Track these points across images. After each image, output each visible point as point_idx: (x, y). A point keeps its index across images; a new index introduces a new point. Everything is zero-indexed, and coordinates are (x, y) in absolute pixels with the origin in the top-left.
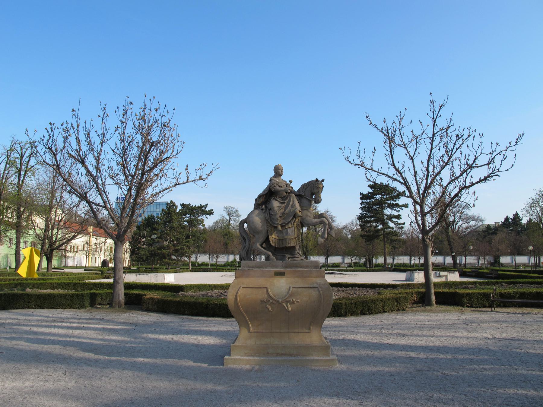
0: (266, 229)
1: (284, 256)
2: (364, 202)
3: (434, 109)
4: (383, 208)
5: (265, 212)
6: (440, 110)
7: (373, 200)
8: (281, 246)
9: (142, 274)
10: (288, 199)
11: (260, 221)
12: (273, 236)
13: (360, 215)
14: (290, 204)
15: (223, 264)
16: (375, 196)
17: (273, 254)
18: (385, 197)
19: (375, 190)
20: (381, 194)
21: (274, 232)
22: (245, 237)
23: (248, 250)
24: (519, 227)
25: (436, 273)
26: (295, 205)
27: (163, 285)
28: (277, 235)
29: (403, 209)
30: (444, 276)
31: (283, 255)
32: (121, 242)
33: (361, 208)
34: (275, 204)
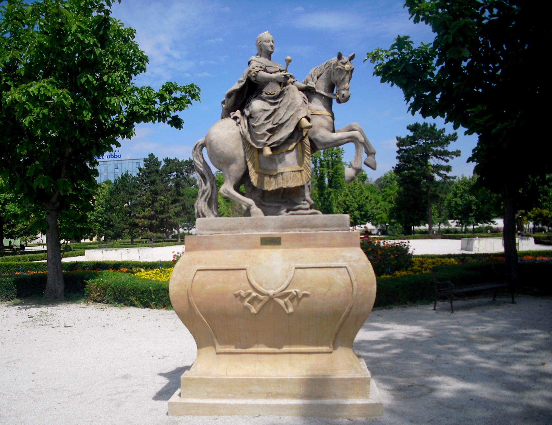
2: (402, 150)
16: (416, 141)
17: (259, 205)
22: (205, 174)
23: (210, 199)
33: (397, 157)
34: (257, 105)
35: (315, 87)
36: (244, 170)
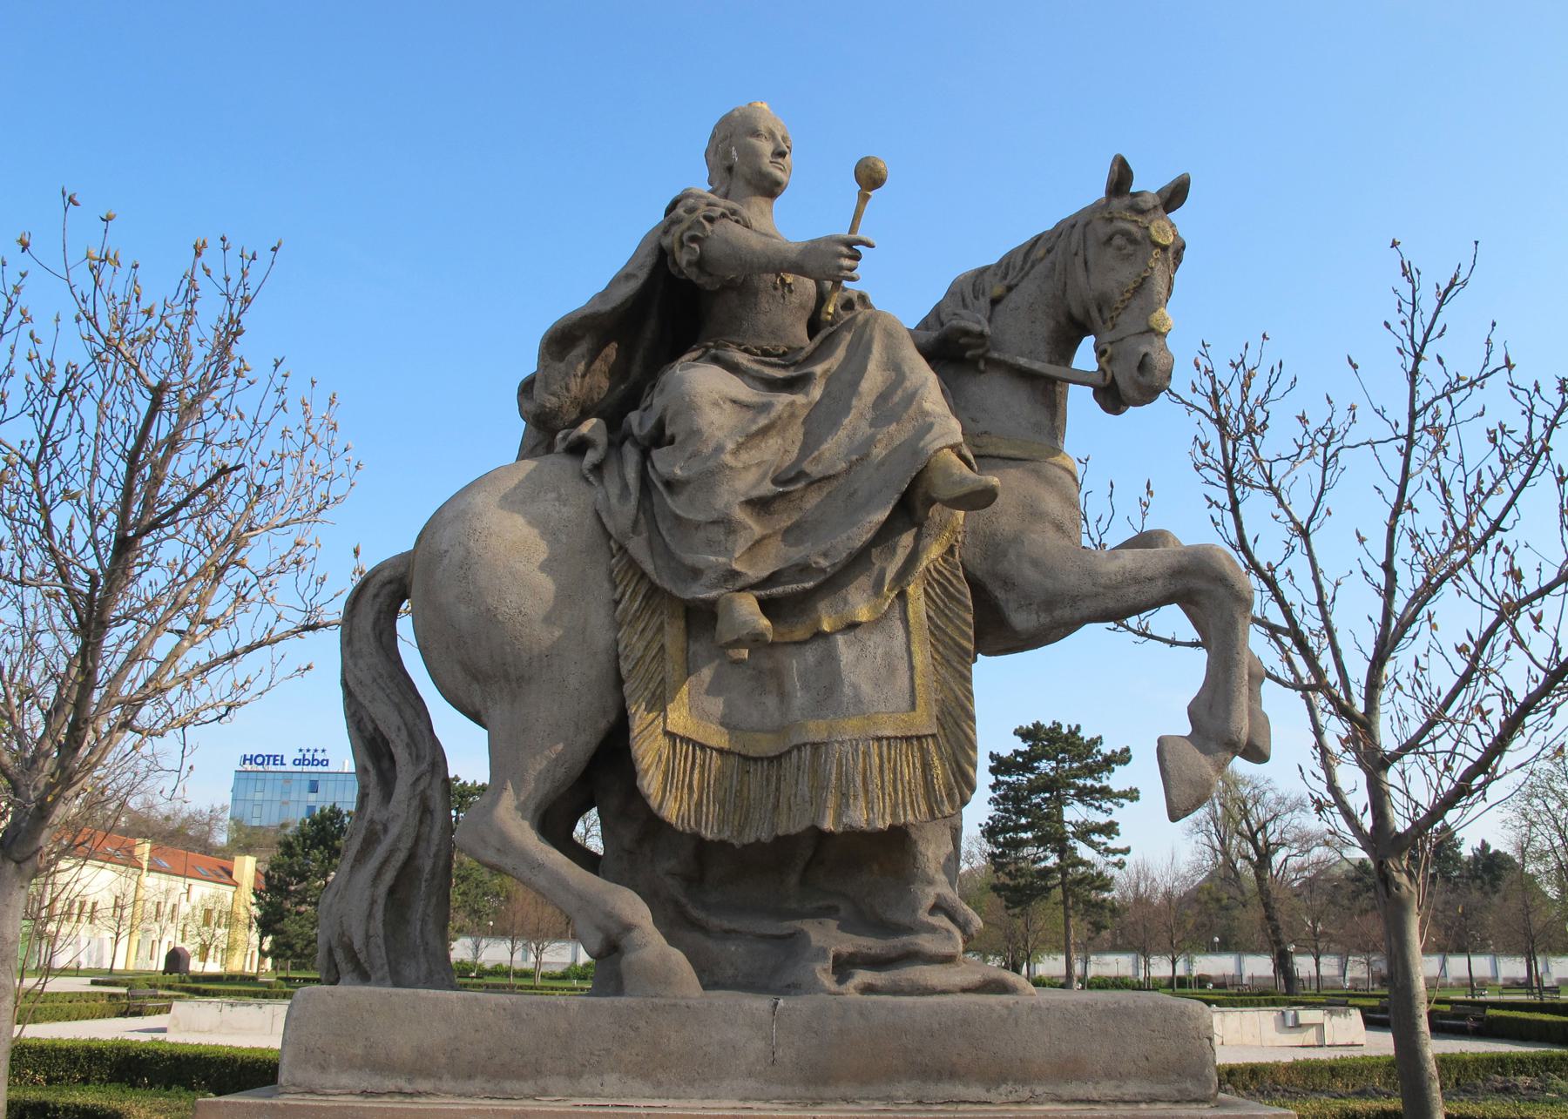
0: (601, 637)
1: (792, 944)
2: (1004, 783)
3: (1414, 304)
4: (1061, 802)
5: (598, 469)
6: (1441, 303)
7: (1032, 777)
8: (758, 832)
9: (243, 1005)
10: (840, 353)
11: (541, 551)
12: (679, 717)
13: (991, 823)
14: (865, 386)
15: (558, 970)
16: (1036, 764)
17: (674, 922)
18: (1067, 766)
19: (1037, 745)
20: (1055, 758)
21: (689, 670)
22: (391, 735)
23: (408, 870)
24: (1455, 867)
25: (1283, 1013)
26: (911, 397)
27: (257, 1060)
28: (716, 706)
29: (1122, 805)
30: (1312, 1025)
31: (787, 926)
32: (18, 862)
33: (992, 800)
35: (987, 330)
36: (612, 717)
